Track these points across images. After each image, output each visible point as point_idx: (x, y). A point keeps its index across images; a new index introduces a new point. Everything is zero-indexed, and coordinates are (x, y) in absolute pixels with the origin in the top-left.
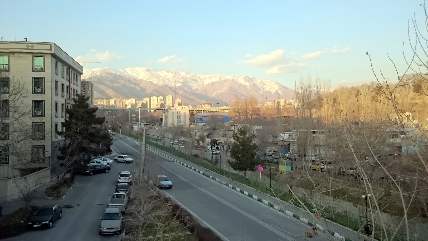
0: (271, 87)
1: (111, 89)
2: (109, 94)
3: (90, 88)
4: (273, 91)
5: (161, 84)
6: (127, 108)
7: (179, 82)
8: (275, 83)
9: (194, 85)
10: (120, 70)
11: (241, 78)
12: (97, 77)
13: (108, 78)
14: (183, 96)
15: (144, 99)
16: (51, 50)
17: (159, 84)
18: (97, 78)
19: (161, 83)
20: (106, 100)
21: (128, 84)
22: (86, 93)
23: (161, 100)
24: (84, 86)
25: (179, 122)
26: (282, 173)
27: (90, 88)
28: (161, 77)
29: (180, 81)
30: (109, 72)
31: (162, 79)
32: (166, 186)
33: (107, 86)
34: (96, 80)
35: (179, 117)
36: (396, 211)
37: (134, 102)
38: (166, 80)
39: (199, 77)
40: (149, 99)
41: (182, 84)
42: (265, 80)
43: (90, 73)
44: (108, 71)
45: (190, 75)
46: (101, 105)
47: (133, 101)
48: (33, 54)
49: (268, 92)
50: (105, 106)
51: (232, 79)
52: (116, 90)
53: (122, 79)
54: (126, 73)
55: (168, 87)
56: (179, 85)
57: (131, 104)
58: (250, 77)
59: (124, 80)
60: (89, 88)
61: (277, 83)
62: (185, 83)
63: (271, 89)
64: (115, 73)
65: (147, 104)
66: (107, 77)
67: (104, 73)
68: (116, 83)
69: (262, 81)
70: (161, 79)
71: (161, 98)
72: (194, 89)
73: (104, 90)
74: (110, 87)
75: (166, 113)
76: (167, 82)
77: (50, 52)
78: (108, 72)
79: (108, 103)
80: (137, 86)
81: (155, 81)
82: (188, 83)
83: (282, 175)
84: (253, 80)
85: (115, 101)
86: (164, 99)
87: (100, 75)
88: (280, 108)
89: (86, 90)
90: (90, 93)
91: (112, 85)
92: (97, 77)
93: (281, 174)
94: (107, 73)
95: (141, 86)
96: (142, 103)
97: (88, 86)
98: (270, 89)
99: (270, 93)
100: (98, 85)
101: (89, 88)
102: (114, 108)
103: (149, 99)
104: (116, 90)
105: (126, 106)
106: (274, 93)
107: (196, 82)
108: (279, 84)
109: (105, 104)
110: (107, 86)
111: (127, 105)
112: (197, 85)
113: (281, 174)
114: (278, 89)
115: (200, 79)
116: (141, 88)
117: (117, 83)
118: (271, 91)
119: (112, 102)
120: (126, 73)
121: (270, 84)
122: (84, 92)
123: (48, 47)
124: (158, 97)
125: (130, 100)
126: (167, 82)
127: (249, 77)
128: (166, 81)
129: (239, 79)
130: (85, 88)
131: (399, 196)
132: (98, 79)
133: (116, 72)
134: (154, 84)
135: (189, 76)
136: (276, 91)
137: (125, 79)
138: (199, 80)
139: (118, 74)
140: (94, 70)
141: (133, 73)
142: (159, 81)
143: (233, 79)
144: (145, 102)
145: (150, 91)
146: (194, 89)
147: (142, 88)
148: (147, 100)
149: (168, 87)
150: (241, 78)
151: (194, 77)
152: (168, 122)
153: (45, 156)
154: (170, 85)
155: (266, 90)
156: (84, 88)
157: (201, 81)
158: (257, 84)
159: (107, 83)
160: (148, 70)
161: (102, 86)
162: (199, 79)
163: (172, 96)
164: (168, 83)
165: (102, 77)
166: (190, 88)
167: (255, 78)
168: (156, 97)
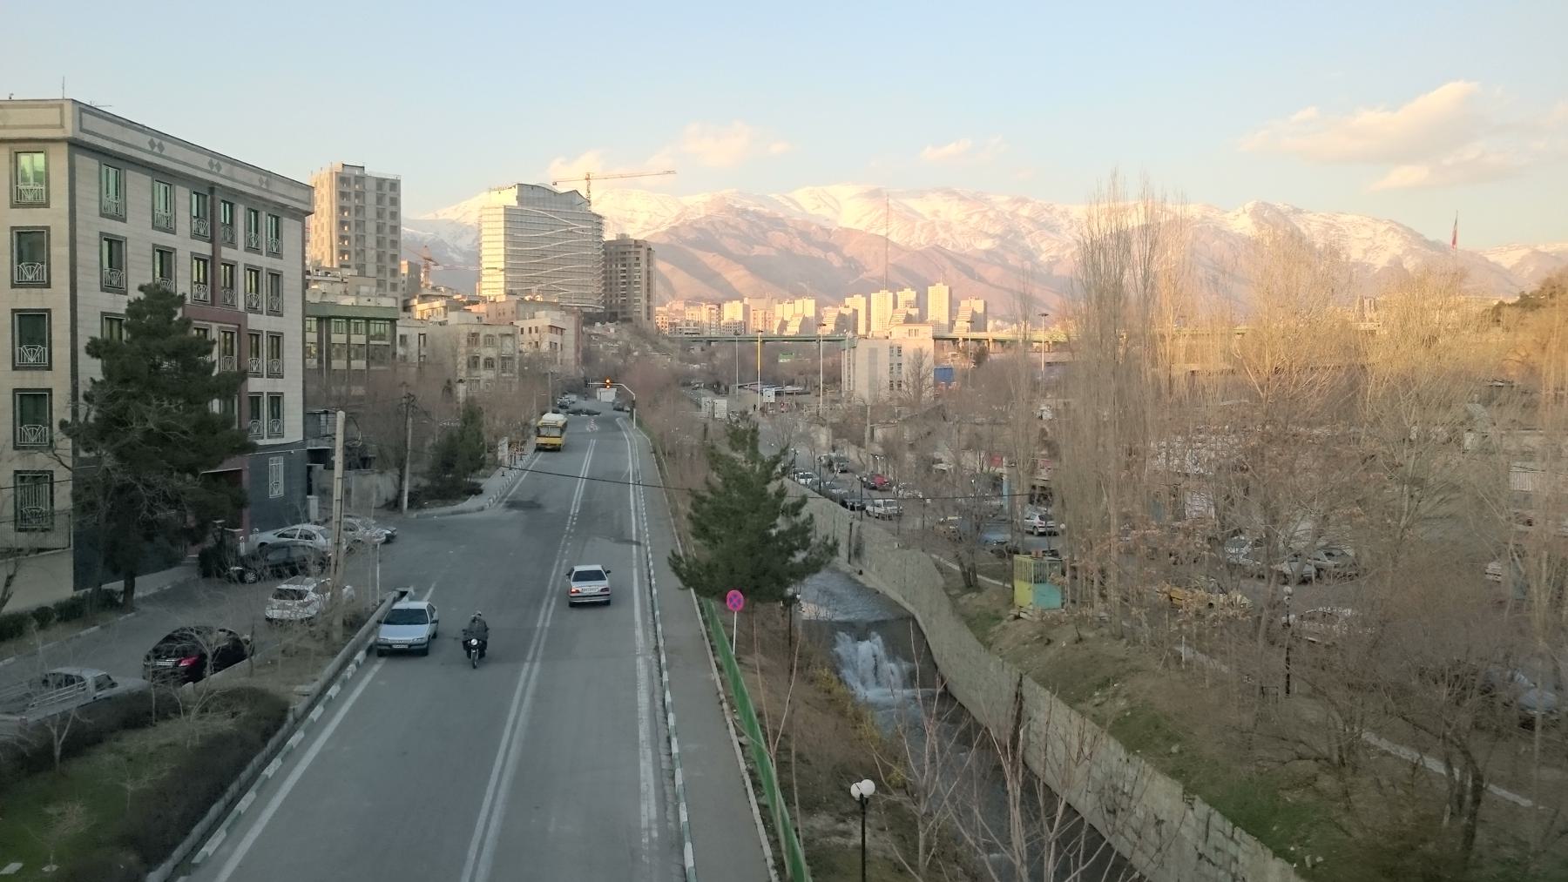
0: (1370, 243)
1: (741, 266)
2: (734, 284)
3: (643, 265)
4: (1381, 261)
5: (920, 245)
6: (785, 334)
7: (988, 235)
8: (1389, 229)
9: (1044, 246)
10: (774, 196)
11: (1240, 210)
12: (695, 226)
13: (732, 227)
14: (997, 287)
15: (847, 299)
16: (62, 126)
17: (911, 244)
18: (696, 229)
19: (920, 240)
20: (709, 306)
21: (799, 247)
22: (630, 283)
23: (908, 303)
24: (624, 259)
25: (895, 387)
26: (1022, 615)
27: (643, 265)
28: (923, 217)
29: (991, 231)
30: (737, 206)
31: (923, 227)
32: (395, 647)
33: (727, 254)
34: (692, 236)
35: (895, 366)
36: (1319, 859)
37: (810, 312)
38: (938, 229)
39: (1065, 214)
40: (864, 299)
41: (997, 242)
42: (1343, 218)
43: (676, 212)
44: (735, 202)
45: (1030, 205)
46: (692, 324)
47: (808, 307)
48: (12, 145)
49: (1355, 264)
50: (706, 328)
51: (1198, 217)
52: (758, 269)
53: (780, 231)
54: (793, 207)
55: (943, 254)
56: (986, 244)
57: (801, 319)
58: (1280, 205)
59: (786, 233)
60: (638, 265)
61: (1399, 225)
62: (1010, 238)
63: (1369, 254)
64: (758, 209)
65: (856, 319)
66: (731, 223)
67: (721, 211)
68: (757, 244)
69: (1331, 222)
70: (918, 224)
71: (909, 294)
72: (1043, 258)
73: (717, 270)
74: (738, 260)
75: (849, 352)
76: (942, 235)
77: (58, 134)
78: (732, 207)
79: (715, 317)
80: (831, 255)
81: (897, 234)
82: (1023, 238)
83: (1019, 621)
84: (1292, 218)
85: (746, 310)
86: (917, 298)
87: (707, 216)
88: (1155, 336)
89: (630, 271)
90: (644, 280)
91: (745, 254)
92: (697, 226)
93: (1017, 617)
94: (730, 209)
95: (847, 252)
96: (836, 314)
97: (638, 259)
98: (1366, 252)
99: (1367, 268)
100: (699, 253)
101: (638, 265)
102: (736, 334)
103: (864, 299)
104: (758, 269)
105: (784, 325)
106: (1383, 268)
107: (1053, 231)
108: (1410, 230)
109: (705, 319)
110: (727, 254)
111: (787, 322)
112: (1057, 243)
113: (1017, 617)
114: (1400, 252)
115: (1071, 221)
116: (845, 259)
117: (763, 245)
118: (1371, 261)
119: (733, 312)
120: (793, 207)
121: (1367, 233)
122: (624, 277)
123: (52, 116)
124: (898, 293)
125: (798, 303)
126: (942, 235)
127: (1271, 207)
128: (937, 234)
129: (1231, 215)
130: (627, 262)
131: (983, 862)
132: (700, 230)
133: (761, 206)
134: (895, 245)
135: (1025, 212)
136: (1390, 261)
137: (790, 230)
138: (1067, 226)
139: (767, 211)
140: (688, 200)
141: (819, 207)
142: (913, 233)
143: (1206, 217)
144: (848, 312)
145: (878, 271)
146: (1043, 258)
147: (846, 260)
148: (857, 302)
149: (943, 254)
150: (1240, 210)
151: (1046, 215)
152: (854, 385)
153: (56, 507)
154: (954, 246)
155: (1348, 258)
156: (624, 265)
157: (1071, 227)
158: (1306, 232)
159: (730, 244)
160: (875, 194)
161: (711, 255)
162: (1065, 223)
163: (947, 287)
164: (944, 240)
165: (712, 223)
166: (1029, 255)
167: (1298, 211)
168: (891, 294)
